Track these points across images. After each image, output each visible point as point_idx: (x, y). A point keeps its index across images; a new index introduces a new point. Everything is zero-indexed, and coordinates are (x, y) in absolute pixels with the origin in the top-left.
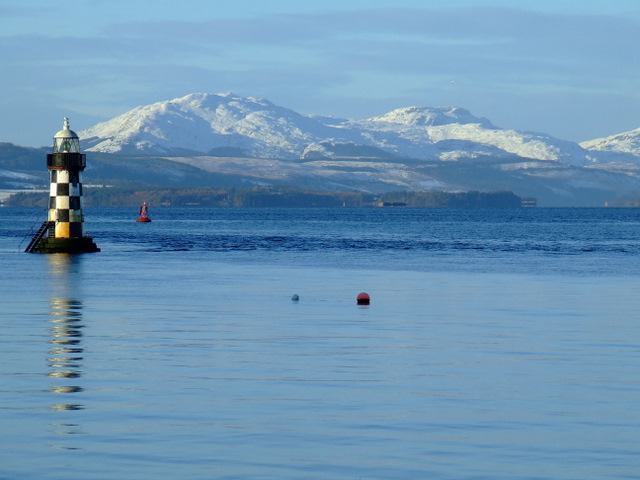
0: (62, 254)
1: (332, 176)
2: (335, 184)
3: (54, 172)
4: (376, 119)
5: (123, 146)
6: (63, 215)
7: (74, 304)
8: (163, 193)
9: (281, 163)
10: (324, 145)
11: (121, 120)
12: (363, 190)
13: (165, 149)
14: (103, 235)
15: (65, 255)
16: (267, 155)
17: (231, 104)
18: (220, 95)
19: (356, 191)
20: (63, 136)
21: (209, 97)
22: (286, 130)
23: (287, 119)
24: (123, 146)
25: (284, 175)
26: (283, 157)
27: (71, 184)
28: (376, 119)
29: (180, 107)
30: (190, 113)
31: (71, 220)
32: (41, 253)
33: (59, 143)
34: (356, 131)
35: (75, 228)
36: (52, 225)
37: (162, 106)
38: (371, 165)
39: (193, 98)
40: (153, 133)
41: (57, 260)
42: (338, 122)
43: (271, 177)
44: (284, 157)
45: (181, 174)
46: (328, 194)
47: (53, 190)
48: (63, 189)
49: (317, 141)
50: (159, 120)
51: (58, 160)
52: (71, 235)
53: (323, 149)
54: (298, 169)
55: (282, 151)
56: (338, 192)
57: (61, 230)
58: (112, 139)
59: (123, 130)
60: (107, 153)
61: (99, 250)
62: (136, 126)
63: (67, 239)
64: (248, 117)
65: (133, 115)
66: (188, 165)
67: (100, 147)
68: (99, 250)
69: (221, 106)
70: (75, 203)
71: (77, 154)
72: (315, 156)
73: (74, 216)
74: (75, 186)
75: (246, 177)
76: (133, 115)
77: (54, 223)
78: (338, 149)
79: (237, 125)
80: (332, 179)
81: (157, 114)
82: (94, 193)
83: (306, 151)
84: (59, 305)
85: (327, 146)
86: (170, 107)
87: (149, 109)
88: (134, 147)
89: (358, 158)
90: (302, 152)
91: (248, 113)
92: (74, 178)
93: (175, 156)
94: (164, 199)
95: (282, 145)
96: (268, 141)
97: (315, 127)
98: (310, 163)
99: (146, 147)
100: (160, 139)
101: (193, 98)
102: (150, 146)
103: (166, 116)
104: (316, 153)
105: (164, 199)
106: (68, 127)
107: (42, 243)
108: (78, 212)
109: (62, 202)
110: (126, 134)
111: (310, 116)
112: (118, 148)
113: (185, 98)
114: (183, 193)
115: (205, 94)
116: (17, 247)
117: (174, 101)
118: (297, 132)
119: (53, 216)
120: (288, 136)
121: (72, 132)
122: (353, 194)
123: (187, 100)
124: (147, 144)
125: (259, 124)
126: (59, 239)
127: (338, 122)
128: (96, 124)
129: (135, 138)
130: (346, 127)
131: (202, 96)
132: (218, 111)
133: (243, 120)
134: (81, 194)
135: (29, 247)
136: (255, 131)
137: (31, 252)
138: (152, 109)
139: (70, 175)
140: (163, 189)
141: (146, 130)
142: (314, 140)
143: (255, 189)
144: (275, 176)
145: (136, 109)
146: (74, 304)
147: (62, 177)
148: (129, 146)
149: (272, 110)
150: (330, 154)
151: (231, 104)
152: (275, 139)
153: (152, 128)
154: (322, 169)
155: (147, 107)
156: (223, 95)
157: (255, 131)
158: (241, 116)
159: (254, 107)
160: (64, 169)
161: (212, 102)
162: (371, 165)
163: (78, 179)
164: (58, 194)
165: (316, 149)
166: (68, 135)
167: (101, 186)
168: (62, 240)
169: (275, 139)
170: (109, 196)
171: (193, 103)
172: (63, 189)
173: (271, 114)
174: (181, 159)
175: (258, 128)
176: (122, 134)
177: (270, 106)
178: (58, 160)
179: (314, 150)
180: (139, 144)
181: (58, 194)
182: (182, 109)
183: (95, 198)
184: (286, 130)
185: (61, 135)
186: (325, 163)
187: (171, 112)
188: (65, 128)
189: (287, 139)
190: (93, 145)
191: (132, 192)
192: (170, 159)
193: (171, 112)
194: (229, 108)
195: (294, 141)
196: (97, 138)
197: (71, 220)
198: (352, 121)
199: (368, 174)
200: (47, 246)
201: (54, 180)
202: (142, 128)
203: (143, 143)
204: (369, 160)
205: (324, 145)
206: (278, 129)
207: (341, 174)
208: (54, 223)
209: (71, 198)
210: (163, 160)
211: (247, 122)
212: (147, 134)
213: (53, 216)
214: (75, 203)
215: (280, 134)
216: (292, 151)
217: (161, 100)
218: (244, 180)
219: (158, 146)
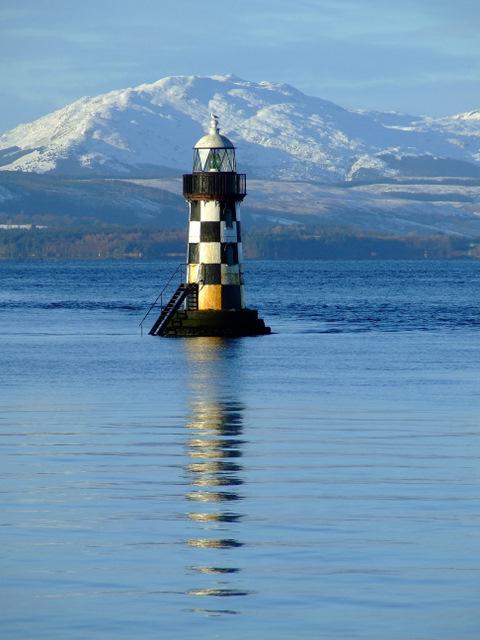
0: (214, 339)
1: (399, 209)
2: (403, 221)
3: (196, 204)
4: (466, 116)
5: (59, 162)
6: (211, 274)
7: (230, 421)
8: (129, 237)
9: (316, 189)
10: (383, 158)
11: (55, 120)
12: (451, 231)
13: (128, 166)
14: (276, 313)
15: (219, 338)
16: (291, 176)
17: (232, 93)
18: (215, 77)
19: (441, 233)
20: (211, 144)
21: (197, 80)
22: (322, 135)
23: (322, 117)
24: (59, 162)
25: (319, 208)
26: (318, 179)
27: (223, 223)
28: (466, 116)
29: (151, 98)
30: (167, 108)
31: (224, 281)
32: (175, 336)
33: (204, 155)
34: (433, 136)
35: (230, 294)
36: (193, 289)
37: (122, 97)
38: (462, 190)
39: (171, 83)
40: (108, 140)
41: (201, 347)
42: (406, 120)
43: (300, 211)
44: (321, 178)
45: (155, 207)
46: (396, 237)
47: (194, 232)
48: (210, 232)
49: (371, 153)
50: (117, 119)
51: (201, 184)
52: (222, 306)
53: (381, 165)
54: (343, 197)
55: (316, 169)
56: (411, 234)
57: (207, 298)
58: (41, 150)
59: (59, 135)
60: (34, 173)
61: (267, 331)
62: (79, 130)
63: (218, 311)
64: (260, 114)
65: (74, 112)
66: (166, 193)
67: (22, 164)
68: (267, 331)
69: (217, 97)
70: (230, 255)
71: (232, 174)
72: (369, 177)
73: (228, 274)
74: (229, 225)
75: (257, 211)
76: (74, 112)
77: (197, 286)
78: (406, 165)
79: (244, 128)
80: (396, 213)
81: (114, 109)
82: (17, 239)
83: (355, 168)
84: (204, 428)
85: (389, 160)
86: (134, 98)
87: (101, 101)
88: (78, 163)
89: (439, 179)
90: (349, 170)
91: (261, 107)
92: (227, 212)
93: (144, 178)
94: (131, 247)
95: (316, 159)
96: (294, 152)
97: (367, 128)
98: (362, 188)
99: (95, 163)
100: (118, 150)
101: (171, 83)
102: (102, 162)
103: (128, 113)
104: (371, 171)
105: (131, 247)
106: (218, 130)
107: (177, 322)
108: (235, 269)
109: (209, 253)
110: (64, 143)
111: (360, 111)
112: (51, 166)
113: (160, 83)
114: (162, 238)
115: (191, 78)
116: (136, 333)
117: (140, 88)
118: (340, 137)
119: (194, 274)
120: (325, 144)
121: (223, 139)
122: (438, 236)
123: (160, 87)
124: (99, 158)
125: (278, 123)
126: (205, 312)
127: (406, 120)
128: (16, 125)
129: (79, 148)
130: (420, 129)
131: (185, 80)
132: (212, 104)
133: (252, 118)
134: (239, 240)
135: (156, 326)
136: (271, 136)
137: (161, 334)
138: (105, 102)
139: (222, 207)
140: (129, 232)
141: (96, 136)
142: (367, 150)
143: (277, 230)
144: (308, 209)
145: (79, 102)
146: (230, 421)
147: (209, 211)
148: (68, 162)
149: (301, 103)
150: (393, 172)
151: (232, 93)
152: (304, 149)
153: (106, 133)
154: (383, 197)
155: (95, 99)
156: (221, 78)
157: (271, 136)
158: (250, 112)
159: (271, 97)
160: (212, 199)
161: (202, 90)
162: (462, 190)
163: (234, 219)
164: (203, 239)
165: (370, 165)
166: (217, 144)
167: (28, 227)
168: (209, 313)
169: (304, 149)
170: (42, 242)
171: (171, 92)
172: (210, 232)
173: (297, 109)
174: (155, 183)
175: (277, 132)
176: (57, 142)
177: (295, 96)
178: (201, 184)
179: (367, 166)
180: (84, 158)
181: (203, 239)
182: (153, 102)
183: (19, 245)
184: (322, 135)
185: (205, 144)
186: (387, 188)
187: (137, 107)
188: (212, 132)
189: (323, 149)
190: (10, 161)
191: (79, 236)
192: (137, 182)
193: (137, 107)
194: (229, 99)
195: (334, 153)
196: (16, 148)
197: (224, 281)
198: (429, 120)
199: (457, 204)
200: (185, 323)
201: (196, 216)
202: (89, 133)
203: (91, 156)
204: (458, 183)
205: (383, 158)
206: (310, 132)
207: (411, 206)
208: (197, 286)
209: (223, 245)
210: (125, 183)
211: (259, 121)
212: (100, 142)
213: (194, 274)
214: (229, 253)
215: (311, 140)
216: (332, 169)
217: (119, 86)
218: (255, 216)
219: (115, 161)
